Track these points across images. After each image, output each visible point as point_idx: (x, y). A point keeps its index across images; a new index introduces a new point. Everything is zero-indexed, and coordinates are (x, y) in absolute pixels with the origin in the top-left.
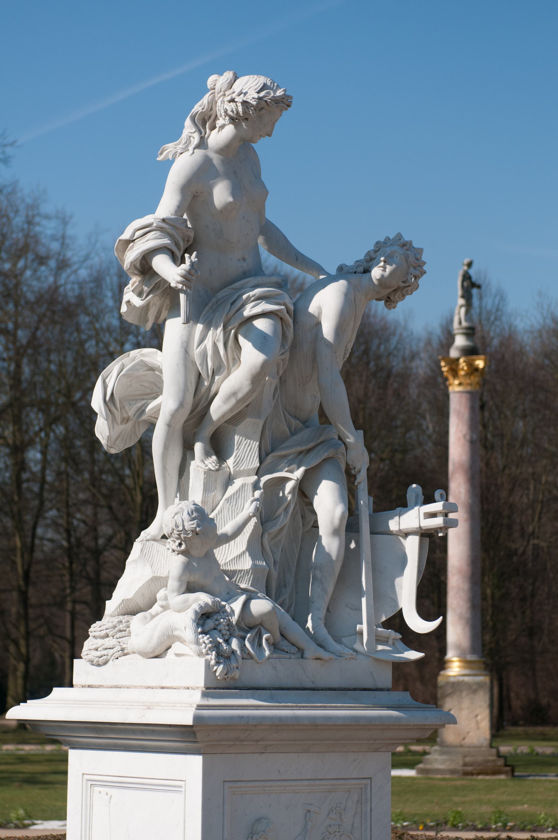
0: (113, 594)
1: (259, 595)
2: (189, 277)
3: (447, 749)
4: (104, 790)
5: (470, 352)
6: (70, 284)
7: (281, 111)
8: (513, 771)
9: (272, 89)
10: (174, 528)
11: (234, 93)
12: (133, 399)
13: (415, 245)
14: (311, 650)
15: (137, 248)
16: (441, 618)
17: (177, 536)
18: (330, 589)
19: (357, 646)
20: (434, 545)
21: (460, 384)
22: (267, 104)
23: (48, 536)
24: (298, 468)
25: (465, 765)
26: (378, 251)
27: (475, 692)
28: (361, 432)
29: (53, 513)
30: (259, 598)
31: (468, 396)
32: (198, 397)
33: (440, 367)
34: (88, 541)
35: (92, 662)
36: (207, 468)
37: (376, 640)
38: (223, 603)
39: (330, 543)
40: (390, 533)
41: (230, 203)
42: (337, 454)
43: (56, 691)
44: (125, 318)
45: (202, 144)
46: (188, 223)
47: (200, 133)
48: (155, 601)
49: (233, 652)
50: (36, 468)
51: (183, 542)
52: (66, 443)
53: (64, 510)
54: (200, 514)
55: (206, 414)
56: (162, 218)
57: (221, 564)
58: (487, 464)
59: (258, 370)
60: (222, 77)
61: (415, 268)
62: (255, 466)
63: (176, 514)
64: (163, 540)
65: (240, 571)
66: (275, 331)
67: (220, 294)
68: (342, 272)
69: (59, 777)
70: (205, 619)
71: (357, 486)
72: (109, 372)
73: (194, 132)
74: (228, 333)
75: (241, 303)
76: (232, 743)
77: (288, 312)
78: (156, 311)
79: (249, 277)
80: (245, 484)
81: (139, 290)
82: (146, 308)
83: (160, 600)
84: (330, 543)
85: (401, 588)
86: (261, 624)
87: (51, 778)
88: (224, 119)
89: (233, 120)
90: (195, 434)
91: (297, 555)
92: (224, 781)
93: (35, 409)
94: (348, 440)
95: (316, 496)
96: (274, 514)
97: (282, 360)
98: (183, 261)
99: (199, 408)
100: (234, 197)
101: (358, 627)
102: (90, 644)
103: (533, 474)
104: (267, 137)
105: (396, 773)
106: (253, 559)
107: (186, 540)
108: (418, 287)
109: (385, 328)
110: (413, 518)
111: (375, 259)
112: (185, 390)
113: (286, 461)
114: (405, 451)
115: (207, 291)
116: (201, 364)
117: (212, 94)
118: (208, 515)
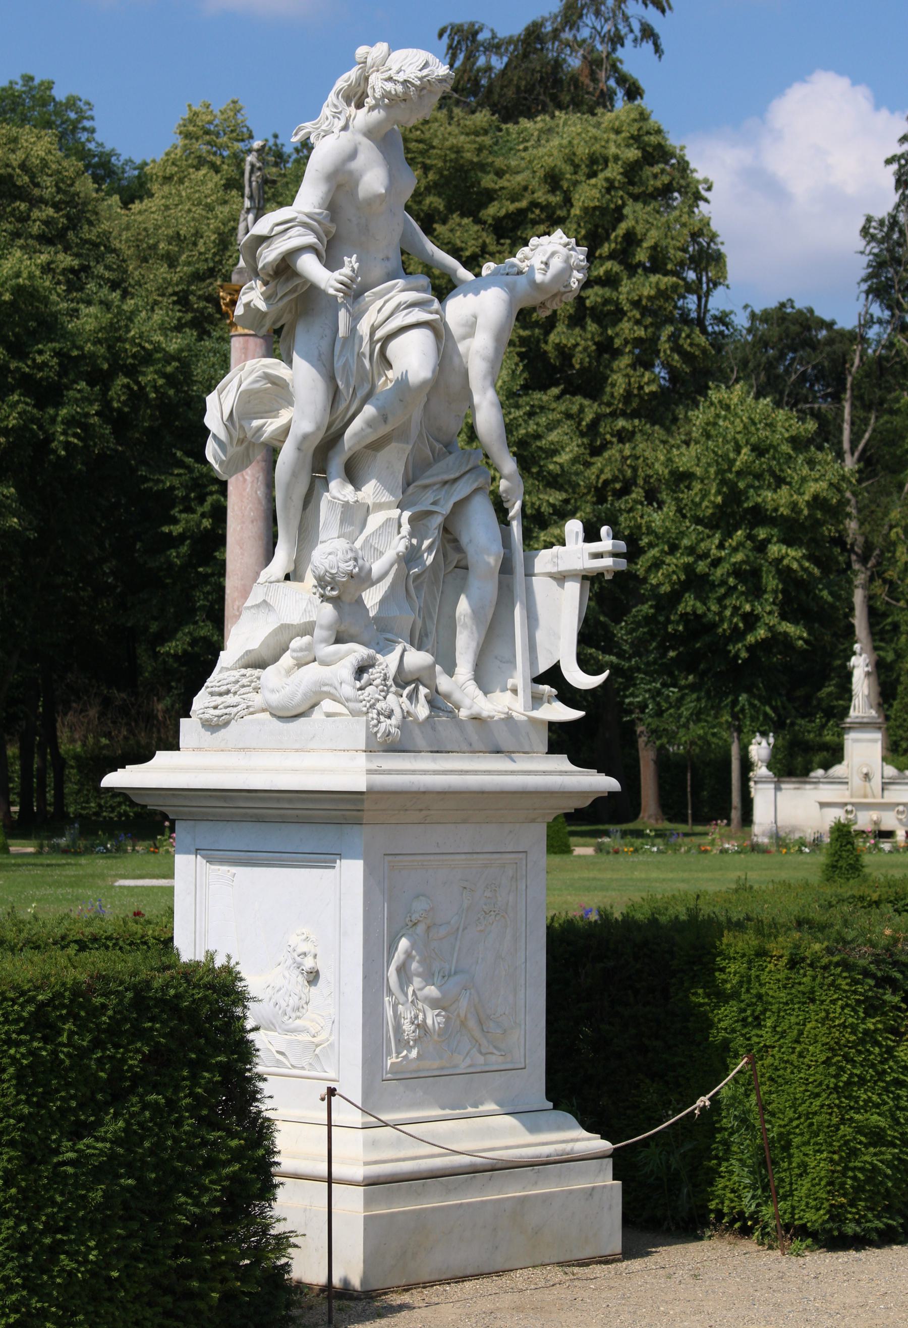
43: (162, 757)
99: (333, 430)
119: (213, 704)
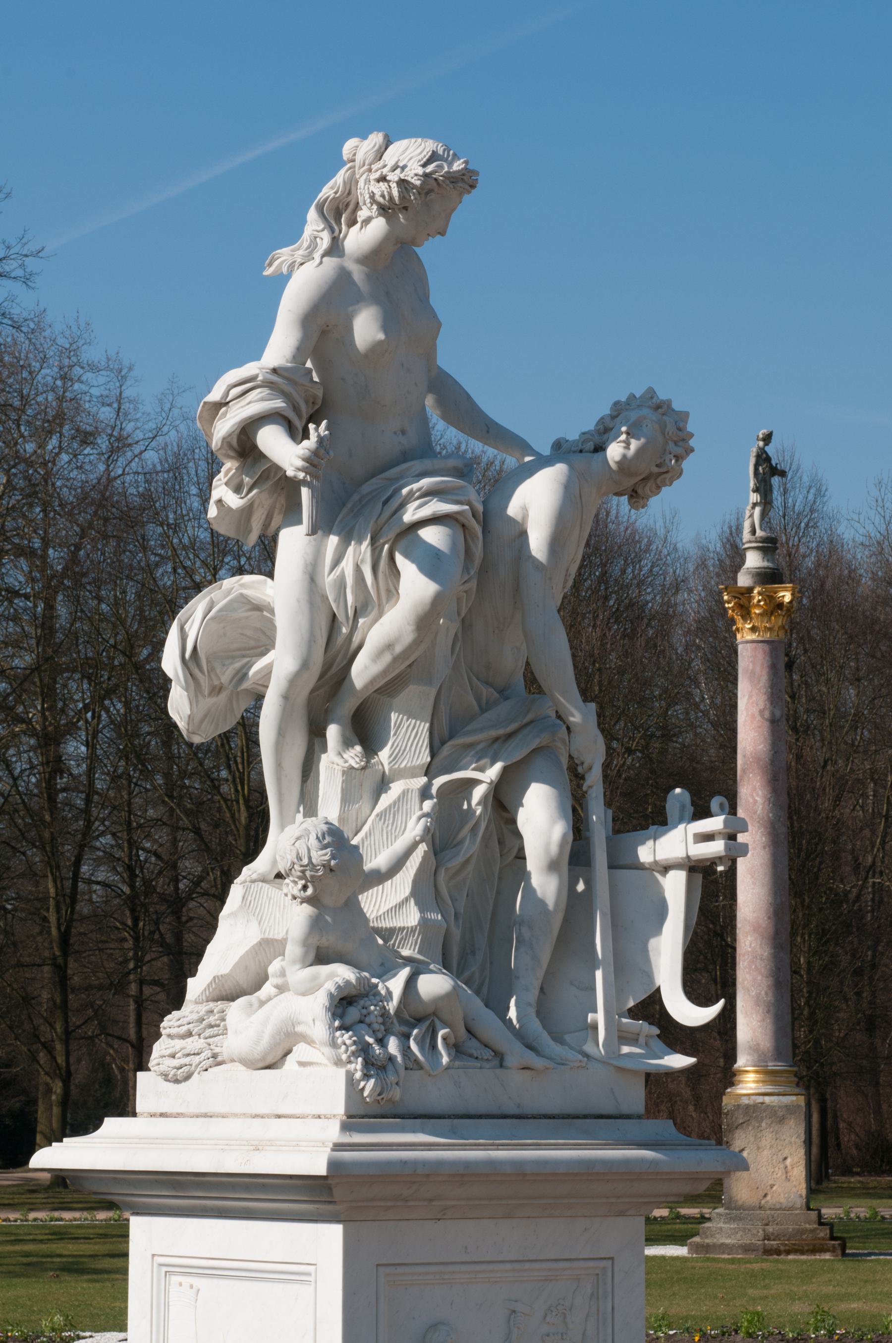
0: (200, 967)
1: (432, 967)
2: (316, 461)
3: (738, 1212)
5: (769, 577)
6: (131, 476)
7: (461, 195)
8: (843, 1247)
9: (446, 160)
10: (295, 860)
11: (385, 166)
12: (228, 656)
13: (676, 406)
14: (516, 1054)
15: (232, 415)
16: (722, 1002)
17: (299, 874)
18: (545, 957)
19: (589, 1048)
20: (713, 886)
21: (753, 629)
22: (438, 184)
23: (99, 875)
24: (493, 763)
25: (767, 1238)
26: (617, 416)
27: (781, 1120)
28: (593, 706)
29: (107, 840)
30: (431, 972)
31: (766, 647)
33: (723, 603)
34: (161, 885)
35: (165, 1076)
36: (347, 765)
37: (619, 1037)
38: (374, 980)
39: (544, 884)
40: (640, 867)
41: (381, 343)
42: (554, 741)
43: (111, 1124)
44: (215, 527)
45: (335, 248)
46: (314, 374)
47: (332, 231)
48: (266, 978)
49: (391, 1059)
50: (79, 769)
51: (309, 884)
52: (126, 729)
53: (125, 835)
54: (336, 839)
55: (344, 679)
56: (272, 366)
57: (371, 918)
58: (799, 757)
59: (427, 607)
60: (366, 142)
61: (676, 443)
62: (424, 761)
63: (298, 839)
64: (277, 880)
65: (402, 929)
66: (454, 545)
67: (366, 488)
68: (561, 451)
69: (117, 1262)
70: (346, 1006)
71: (586, 792)
72: (189, 613)
73: (323, 230)
74: (379, 549)
75: (400, 501)
76: (390, 1204)
77: (474, 516)
78: (264, 517)
79: (413, 459)
80: (408, 790)
81: (235, 482)
82: (247, 511)
83: (273, 976)
84: (544, 884)
85: (659, 953)
86: (434, 1014)
87: (106, 1263)
88: (370, 209)
89: (385, 210)
90: (327, 711)
91: (491, 904)
92: (378, 1265)
93: (77, 676)
94: (572, 719)
95: (521, 809)
96: (454, 838)
97: (466, 592)
98: (306, 435)
100: (386, 333)
101: (590, 1016)
102: (163, 1047)
103: (873, 771)
104: (439, 236)
105: (652, 1251)
106: (422, 911)
107: (314, 880)
108: (681, 474)
109: (633, 538)
110: (678, 842)
111: (612, 429)
112: (311, 641)
113: (472, 753)
114: (667, 735)
115: (344, 484)
116: (337, 600)
117: (350, 168)
118: (348, 841)
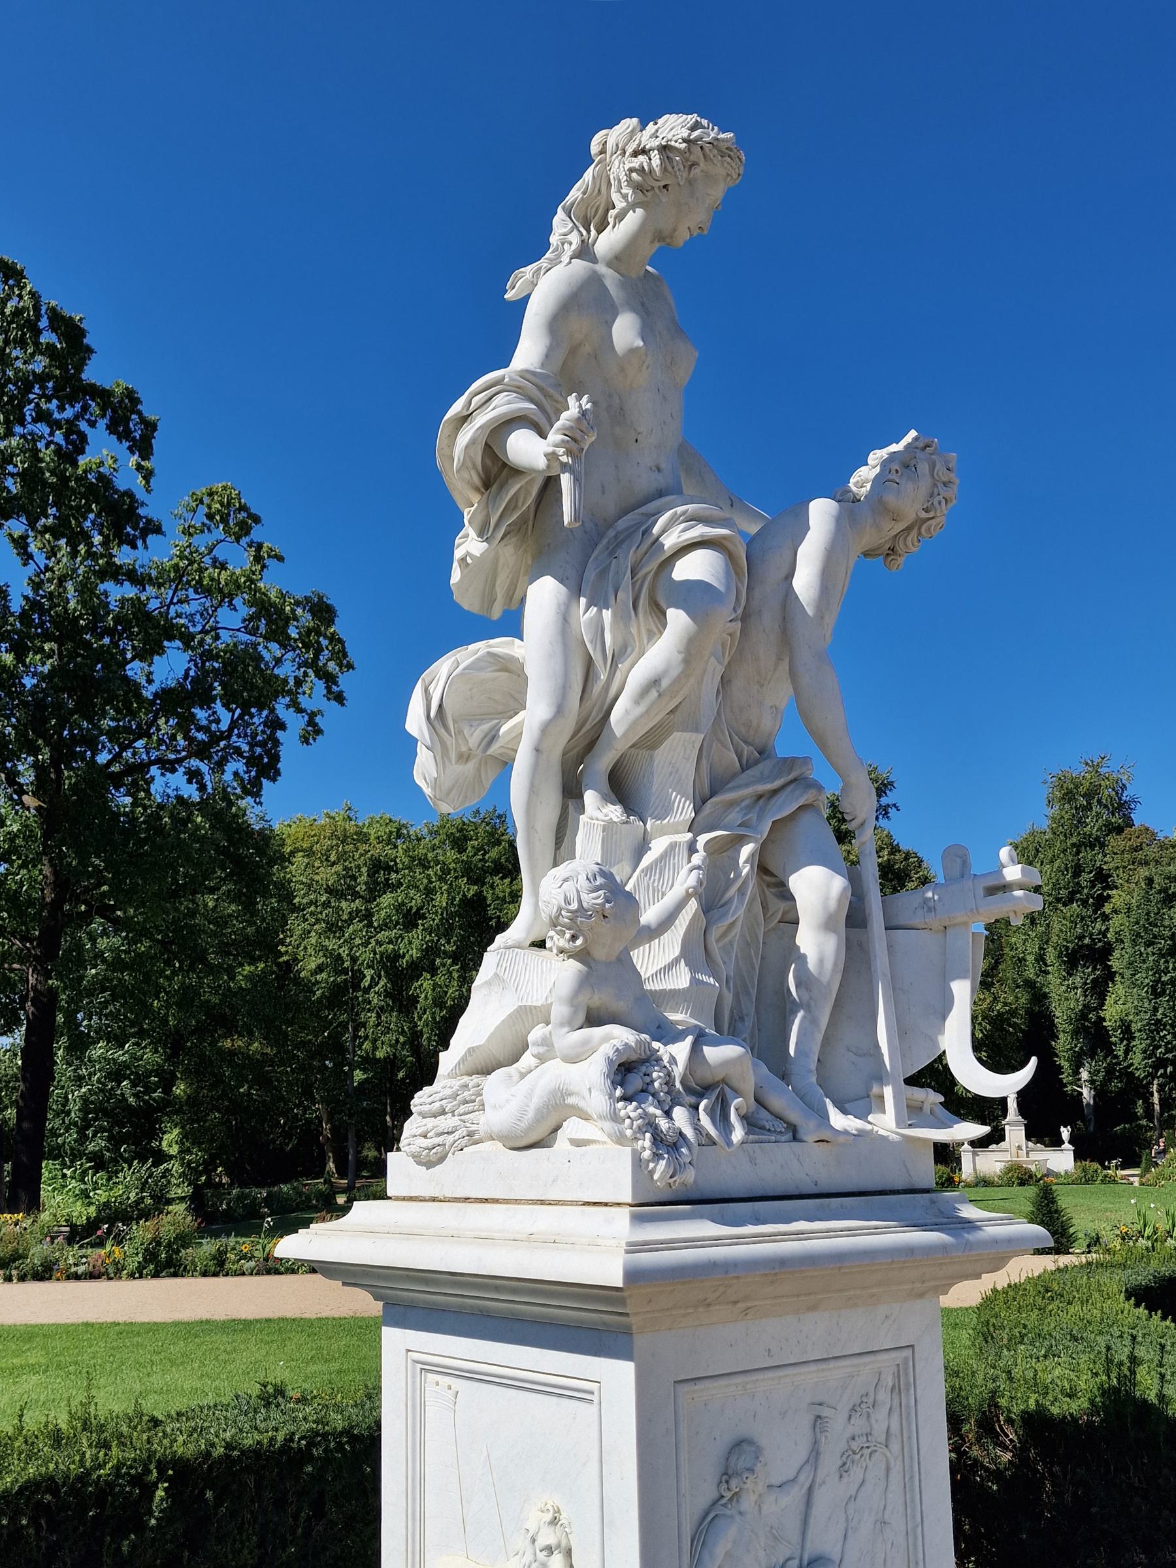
0: (452, 1041)
2: (578, 435)
4: (445, 1380)
12: (473, 719)
16: (1034, 1060)
32: (588, 704)
35: (416, 1157)
37: (908, 1106)
41: (638, 348)
43: (361, 1209)
63: (565, 880)
67: (622, 524)
70: (628, 1073)
86: (724, 1081)
99: (588, 726)
119: (420, 1131)
